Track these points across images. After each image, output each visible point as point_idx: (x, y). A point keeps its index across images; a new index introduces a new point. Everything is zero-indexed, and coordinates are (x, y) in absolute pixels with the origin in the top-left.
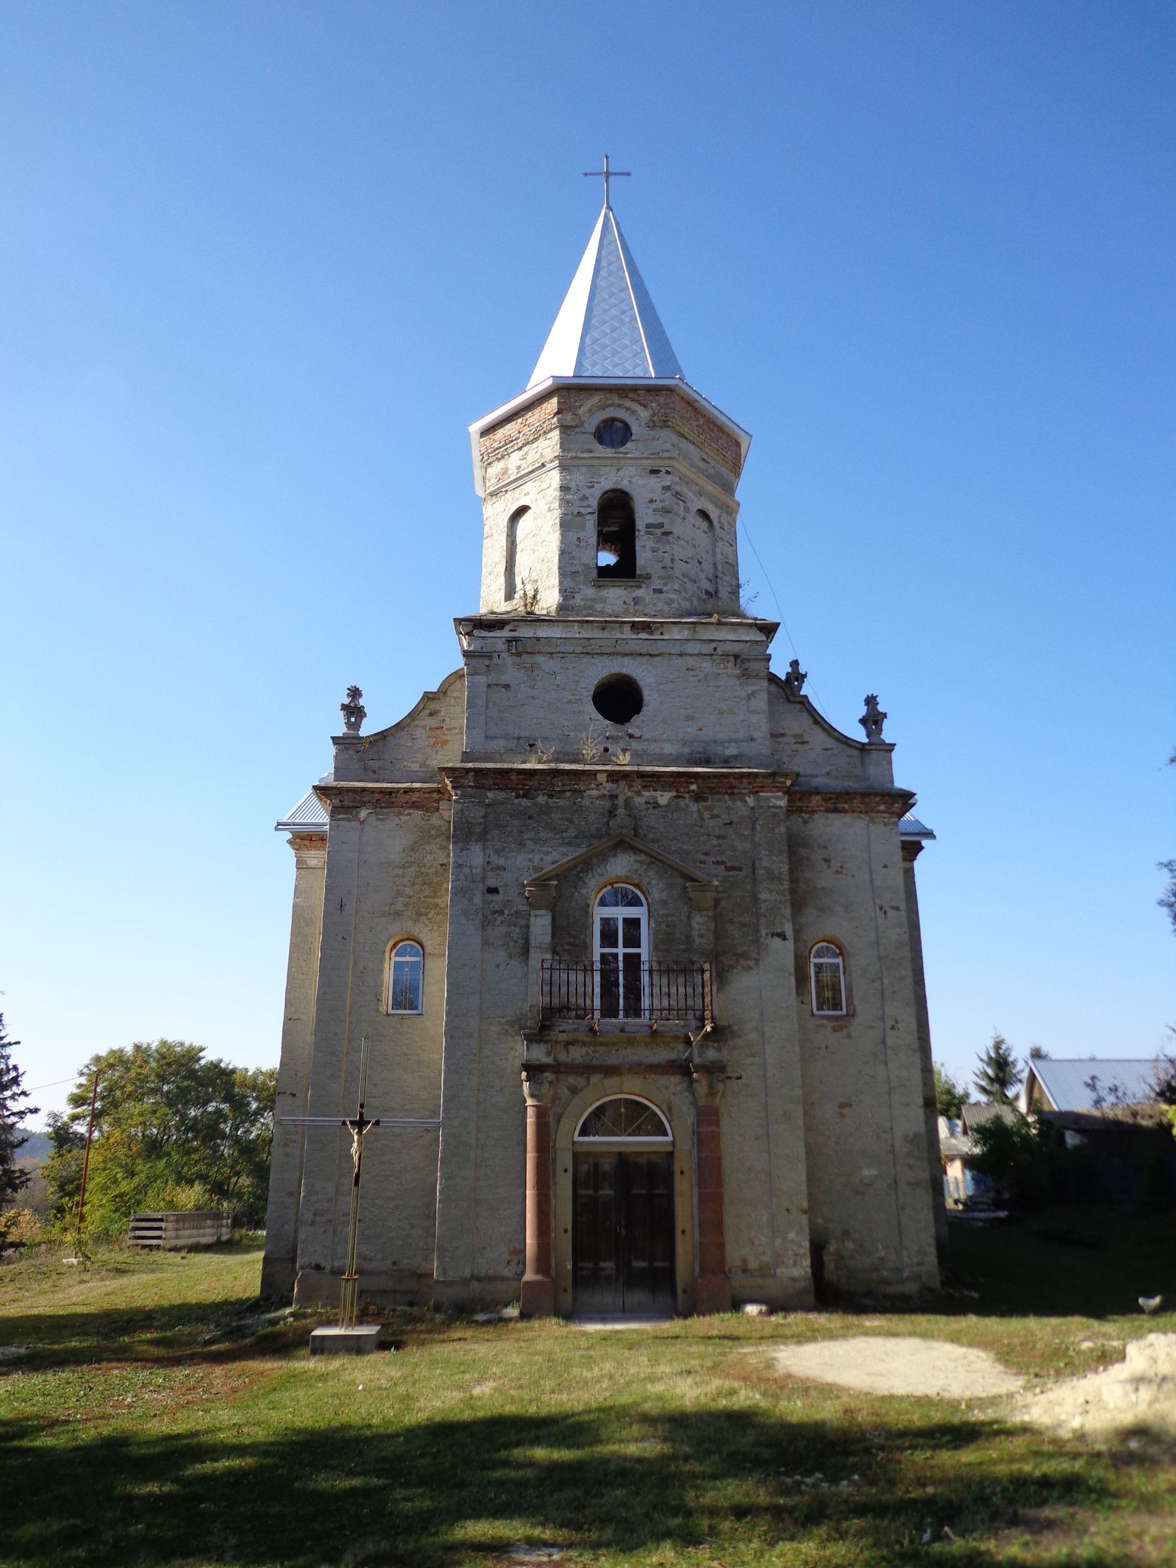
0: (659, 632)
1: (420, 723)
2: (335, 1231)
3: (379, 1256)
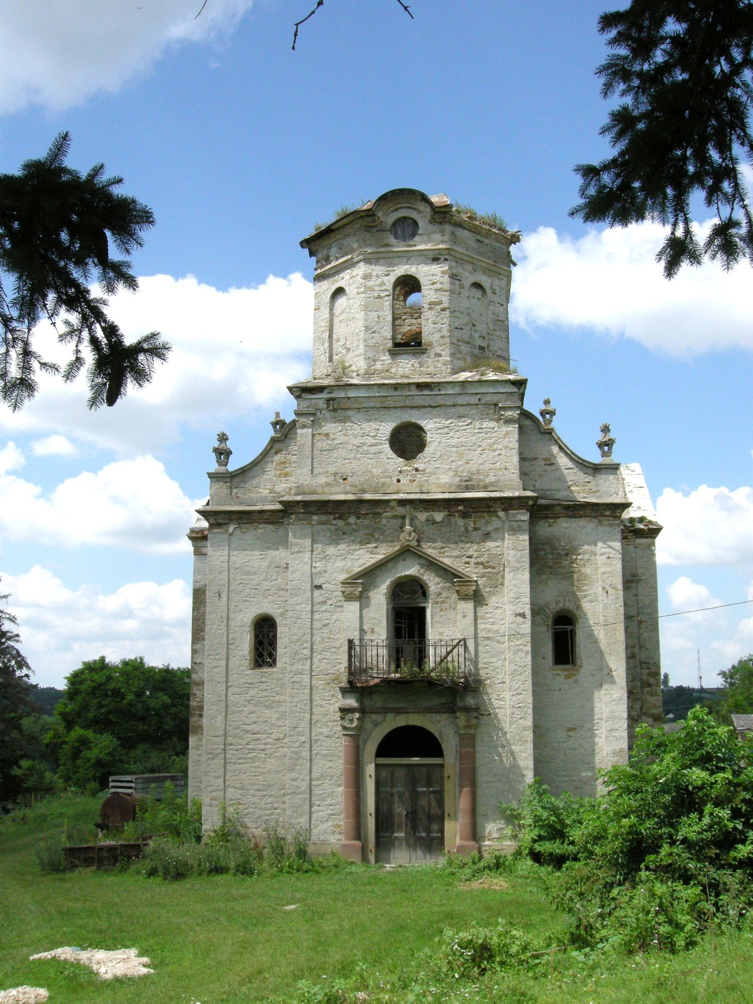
0: (437, 389)
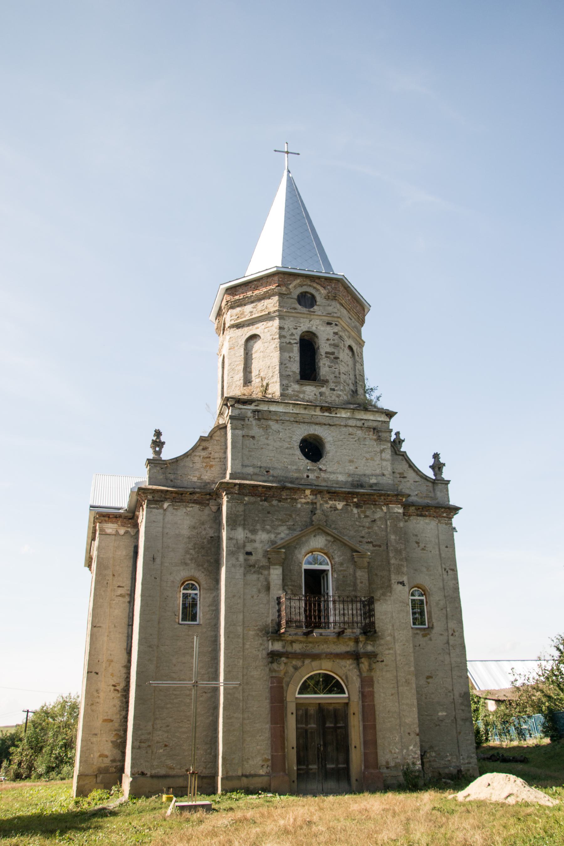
0: (335, 412)
1: (198, 454)
2: (152, 752)
3: (179, 767)
